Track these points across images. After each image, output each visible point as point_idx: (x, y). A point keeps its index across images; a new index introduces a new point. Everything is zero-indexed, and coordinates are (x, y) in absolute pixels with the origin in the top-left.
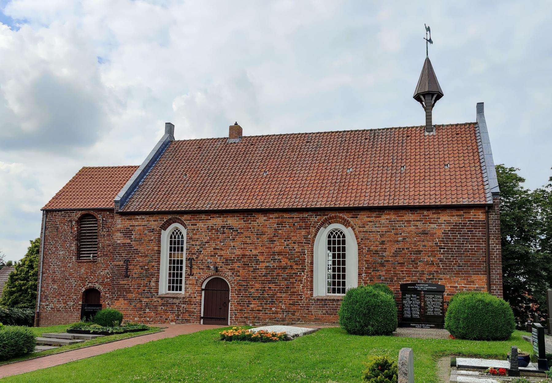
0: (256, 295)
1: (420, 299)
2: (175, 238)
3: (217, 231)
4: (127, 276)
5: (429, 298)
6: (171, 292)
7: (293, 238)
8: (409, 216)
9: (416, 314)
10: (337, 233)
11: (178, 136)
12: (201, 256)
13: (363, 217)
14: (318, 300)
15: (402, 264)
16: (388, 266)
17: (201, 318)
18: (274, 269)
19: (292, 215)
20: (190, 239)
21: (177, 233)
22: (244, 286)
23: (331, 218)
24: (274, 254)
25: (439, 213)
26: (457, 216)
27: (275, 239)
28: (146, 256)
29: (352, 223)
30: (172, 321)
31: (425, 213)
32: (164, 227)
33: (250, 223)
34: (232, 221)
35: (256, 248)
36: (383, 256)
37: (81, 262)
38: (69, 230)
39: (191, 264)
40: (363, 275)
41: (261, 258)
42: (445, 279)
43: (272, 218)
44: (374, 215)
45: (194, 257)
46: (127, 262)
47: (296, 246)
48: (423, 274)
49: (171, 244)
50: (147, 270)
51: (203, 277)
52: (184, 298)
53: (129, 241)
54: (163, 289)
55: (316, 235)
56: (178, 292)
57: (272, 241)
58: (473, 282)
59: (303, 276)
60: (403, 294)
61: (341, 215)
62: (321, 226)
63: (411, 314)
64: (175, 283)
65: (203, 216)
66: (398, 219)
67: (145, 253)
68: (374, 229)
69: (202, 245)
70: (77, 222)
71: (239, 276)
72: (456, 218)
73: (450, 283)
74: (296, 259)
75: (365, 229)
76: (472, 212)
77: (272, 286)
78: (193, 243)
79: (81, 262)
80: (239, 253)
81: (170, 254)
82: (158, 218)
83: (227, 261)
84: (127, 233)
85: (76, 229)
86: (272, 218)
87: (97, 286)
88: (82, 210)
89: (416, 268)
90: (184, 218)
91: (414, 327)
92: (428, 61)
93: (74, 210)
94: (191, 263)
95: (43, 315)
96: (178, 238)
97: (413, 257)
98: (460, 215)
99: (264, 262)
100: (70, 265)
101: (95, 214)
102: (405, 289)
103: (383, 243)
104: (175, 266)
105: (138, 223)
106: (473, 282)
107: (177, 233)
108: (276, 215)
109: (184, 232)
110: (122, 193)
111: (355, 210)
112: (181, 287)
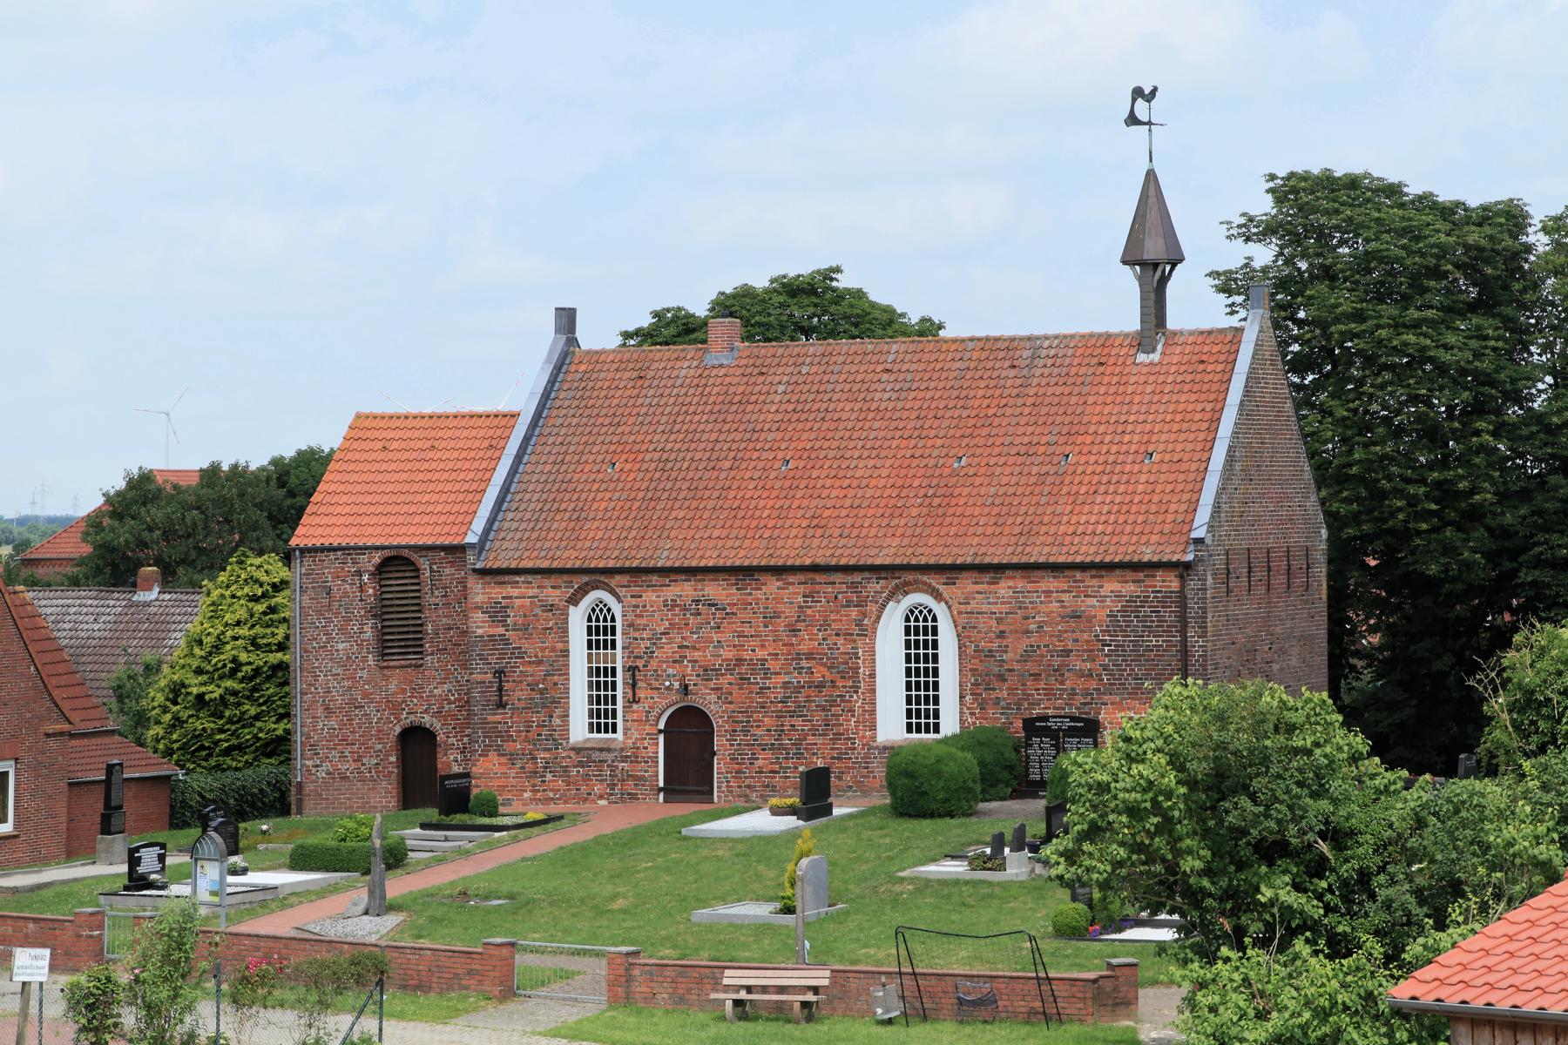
4: (501, 705)
6: (595, 735)
8: (1050, 583)
12: (654, 664)
13: (967, 584)
14: (885, 748)
15: (1036, 676)
16: (1012, 680)
17: (660, 790)
23: (906, 584)
27: (800, 626)
28: (540, 662)
30: (601, 797)
31: (1078, 575)
32: (574, 600)
34: (715, 590)
35: (763, 646)
41: (773, 665)
44: (987, 577)
45: (640, 663)
46: (499, 673)
47: (841, 641)
48: (1073, 694)
49: (590, 634)
50: (542, 692)
51: (661, 707)
53: (501, 630)
54: (579, 729)
55: (879, 617)
56: (610, 735)
57: (794, 631)
60: (1028, 738)
61: (925, 578)
62: (888, 599)
64: (602, 719)
65: (655, 578)
66: (1030, 586)
68: (985, 608)
69: (655, 639)
70: (372, 574)
72: (1131, 587)
74: (842, 667)
77: (798, 722)
78: (637, 635)
80: (730, 655)
81: (590, 655)
82: (559, 580)
83: (707, 672)
84: (498, 613)
87: (427, 721)
88: (383, 548)
89: (1062, 683)
92: (1151, 176)
96: (605, 620)
97: (1057, 662)
100: (365, 674)
101: (414, 556)
102: (1033, 727)
104: (601, 678)
105: (520, 593)
108: (801, 577)
109: (617, 609)
110: (478, 525)
111: (951, 571)
112: (614, 725)
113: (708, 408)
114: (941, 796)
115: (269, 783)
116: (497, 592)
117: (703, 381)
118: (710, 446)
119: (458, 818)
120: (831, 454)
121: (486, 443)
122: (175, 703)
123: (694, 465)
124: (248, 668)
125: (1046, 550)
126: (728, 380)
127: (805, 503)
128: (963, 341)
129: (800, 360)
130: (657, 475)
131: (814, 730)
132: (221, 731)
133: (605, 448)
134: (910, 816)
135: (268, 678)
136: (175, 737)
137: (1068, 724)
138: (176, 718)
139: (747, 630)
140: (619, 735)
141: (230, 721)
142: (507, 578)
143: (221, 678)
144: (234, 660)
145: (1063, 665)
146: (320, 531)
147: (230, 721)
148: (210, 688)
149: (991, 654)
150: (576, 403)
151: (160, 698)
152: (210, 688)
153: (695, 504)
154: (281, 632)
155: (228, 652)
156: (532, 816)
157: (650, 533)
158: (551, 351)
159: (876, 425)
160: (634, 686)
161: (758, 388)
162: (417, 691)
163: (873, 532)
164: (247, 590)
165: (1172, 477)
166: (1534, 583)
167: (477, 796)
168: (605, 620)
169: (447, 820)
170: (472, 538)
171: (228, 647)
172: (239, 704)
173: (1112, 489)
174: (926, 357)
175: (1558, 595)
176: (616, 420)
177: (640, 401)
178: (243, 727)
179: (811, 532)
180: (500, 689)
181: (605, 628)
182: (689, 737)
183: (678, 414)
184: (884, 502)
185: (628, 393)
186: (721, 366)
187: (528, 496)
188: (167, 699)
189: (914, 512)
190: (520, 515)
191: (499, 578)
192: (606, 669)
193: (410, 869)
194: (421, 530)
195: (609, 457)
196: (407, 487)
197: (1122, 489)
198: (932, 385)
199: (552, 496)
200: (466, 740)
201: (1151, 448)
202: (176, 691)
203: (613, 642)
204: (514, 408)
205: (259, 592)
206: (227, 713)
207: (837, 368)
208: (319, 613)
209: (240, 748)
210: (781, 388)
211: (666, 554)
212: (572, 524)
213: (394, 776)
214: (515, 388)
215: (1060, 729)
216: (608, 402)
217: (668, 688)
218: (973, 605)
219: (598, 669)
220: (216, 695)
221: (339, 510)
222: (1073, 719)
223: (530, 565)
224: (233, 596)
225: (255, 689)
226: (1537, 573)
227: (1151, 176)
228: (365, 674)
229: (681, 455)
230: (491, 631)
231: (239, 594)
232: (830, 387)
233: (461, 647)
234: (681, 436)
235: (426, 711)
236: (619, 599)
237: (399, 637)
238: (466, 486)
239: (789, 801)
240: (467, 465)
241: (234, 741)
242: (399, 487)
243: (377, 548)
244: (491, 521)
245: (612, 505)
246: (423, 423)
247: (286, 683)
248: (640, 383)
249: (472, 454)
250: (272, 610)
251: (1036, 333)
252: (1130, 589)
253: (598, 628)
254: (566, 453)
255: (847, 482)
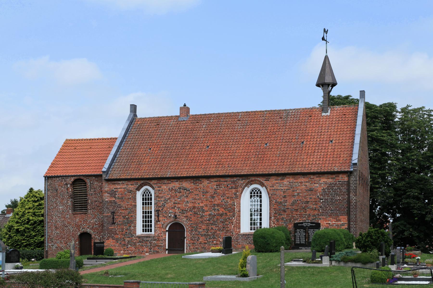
0: (203, 233)
1: (305, 232)
2: (146, 196)
3: (176, 191)
4: (114, 223)
5: (311, 231)
6: (145, 233)
7: (227, 195)
8: (302, 179)
9: (303, 242)
10: (256, 191)
11: (140, 114)
12: (165, 209)
13: (273, 180)
14: (244, 235)
15: (297, 210)
16: (288, 212)
17: (167, 250)
18: (215, 215)
19: (226, 180)
20: (157, 197)
21: (147, 193)
22: (194, 228)
23: (252, 181)
24: (214, 206)
25: (320, 177)
26: (331, 178)
27: (215, 195)
28: (127, 209)
29: (265, 184)
30: (147, 252)
31: (312, 177)
32: (138, 189)
33: (198, 185)
34: (186, 184)
35: (202, 202)
36: (285, 205)
37: (76, 214)
38: (66, 190)
39: (158, 214)
40: (272, 218)
41: (206, 209)
42: (323, 219)
43: (213, 182)
44: (280, 178)
45: (160, 209)
46: (113, 213)
47: (229, 200)
48: (309, 216)
49: (143, 200)
50: (127, 219)
51: (167, 223)
52: (154, 237)
53: (114, 199)
54: (139, 231)
55: (242, 192)
56: (150, 233)
57: (213, 197)
58: (340, 220)
59: (234, 220)
60: (296, 230)
61: (258, 179)
62: (245, 186)
63: (300, 241)
64: (147, 227)
65: (166, 181)
66: (295, 181)
67: (125, 207)
68: (279, 188)
69: (166, 201)
70: (71, 185)
71: (191, 221)
72: (331, 180)
73: (326, 221)
74: (229, 209)
75: (273, 188)
76: (341, 176)
77: (214, 227)
78: (159, 200)
79: (76, 214)
80: (191, 205)
81: (143, 207)
82: (133, 182)
83: (183, 211)
84: (113, 193)
85: (70, 190)
86: (213, 182)
87: (88, 230)
88: (74, 176)
89: (306, 212)
90: (152, 183)
91: (301, 249)
92: (326, 58)
93: (69, 176)
94: (158, 213)
95: (50, 252)
96: (148, 196)
97: (304, 205)
98: (333, 178)
99: (208, 211)
100: (68, 216)
101: (85, 179)
102: (297, 226)
103: (285, 197)
104: (147, 216)
105: (120, 187)
106: (340, 220)
107: (147, 193)
108: (216, 179)
109: (153, 192)
110: (106, 166)
111: (268, 176)
112: (151, 229)
113: (181, 132)
114: (274, 245)
115: (38, 254)
116: (113, 187)
117: (178, 125)
118: (182, 143)
119: (100, 256)
120: (222, 144)
121: (108, 146)
122: (10, 232)
123: (177, 148)
124: (32, 221)
125: (300, 169)
126: (186, 124)
127: (215, 158)
128: (263, 111)
129: (210, 119)
130: (165, 151)
131: (219, 230)
132: (24, 240)
133: (147, 144)
134: (263, 252)
135: (39, 225)
136: (9, 241)
137: (310, 224)
138: (10, 236)
139: (197, 197)
140: (153, 232)
141: (27, 237)
142: (116, 182)
143: (24, 224)
144: (28, 219)
145: (306, 206)
146: (54, 172)
147: (27, 237)
148: (21, 227)
149: (281, 203)
150: (137, 132)
151: (5, 231)
152: (21, 227)
153: (178, 159)
154: (43, 211)
155: (26, 217)
156: (125, 256)
157: (164, 168)
158: (129, 117)
159: (237, 135)
160: (158, 216)
161: (196, 127)
162: (85, 221)
163: (239, 165)
164: (32, 199)
165: (340, 147)
166: (407, 203)
167: (106, 250)
168: (148, 196)
169: (96, 257)
170: (104, 170)
171: (26, 215)
172: (29, 232)
173: (320, 151)
174: (251, 116)
175: (414, 206)
176: (150, 136)
177: (158, 131)
178: (31, 239)
179: (218, 166)
180: (113, 218)
181: (148, 198)
182: (177, 234)
183: (171, 134)
184: (242, 157)
185: (154, 129)
186: (184, 121)
187: (122, 158)
188: (8, 231)
189: (253, 159)
190: (120, 164)
191: (113, 182)
192: (148, 212)
193: (84, 269)
194: (87, 171)
195: (148, 147)
196: (82, 159)
197: (323, 151)
198: (254, 124)
199: (130, 158)
200: (101, 236)
201: (331, 139)
202: (10, 228)
203: (151, 203)
204: (117, 137)
205: (36, 200)
206: (26, 235)
207: (222, 120)
208: (54, 197)
209: (30, 245)
210: (204, 126)
211: (169, 173)
212: (137, 166)
213: (78, 248)
214: (115, 130)
215: (307, 226)
216: (147, 132)
217: (170, 217)
218: (275, 187)
219: (146, 212)
220: (22, 229)
221: (60, 166)
222: (311, 223)
223: (124, 177)
224: (28, 201)
225: (34, 228)
226: (408, 200)
227: (326, 58)
228: (68, 216)
229: (172, 145)
230: (111, 199)
231: (30, 200)
232: (220, 125)
233: (101, 206)
234: (172, 140)
235: (88, 228)
236: (153, 188)
237: (80, 204)
238: (101, 158)
239: (219, 248)
240: (102, 152)
241: (28, 243)
242: (80, 159)
243: (72, 176)
244: (110, 165)
245: (150, 160)
246: (88, 141)
247: (43, 227)
248: (158, 126)
249: (103, 149)
250: (40, 205)
251: (287, 109)
252: (330, 181)
253: (146, 198)
254: (134, 146)
255: (228, 152)
